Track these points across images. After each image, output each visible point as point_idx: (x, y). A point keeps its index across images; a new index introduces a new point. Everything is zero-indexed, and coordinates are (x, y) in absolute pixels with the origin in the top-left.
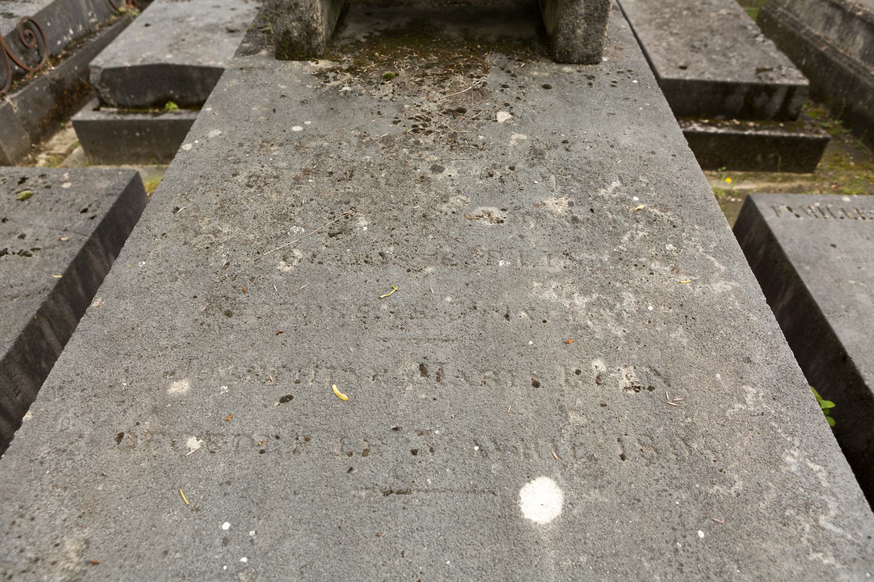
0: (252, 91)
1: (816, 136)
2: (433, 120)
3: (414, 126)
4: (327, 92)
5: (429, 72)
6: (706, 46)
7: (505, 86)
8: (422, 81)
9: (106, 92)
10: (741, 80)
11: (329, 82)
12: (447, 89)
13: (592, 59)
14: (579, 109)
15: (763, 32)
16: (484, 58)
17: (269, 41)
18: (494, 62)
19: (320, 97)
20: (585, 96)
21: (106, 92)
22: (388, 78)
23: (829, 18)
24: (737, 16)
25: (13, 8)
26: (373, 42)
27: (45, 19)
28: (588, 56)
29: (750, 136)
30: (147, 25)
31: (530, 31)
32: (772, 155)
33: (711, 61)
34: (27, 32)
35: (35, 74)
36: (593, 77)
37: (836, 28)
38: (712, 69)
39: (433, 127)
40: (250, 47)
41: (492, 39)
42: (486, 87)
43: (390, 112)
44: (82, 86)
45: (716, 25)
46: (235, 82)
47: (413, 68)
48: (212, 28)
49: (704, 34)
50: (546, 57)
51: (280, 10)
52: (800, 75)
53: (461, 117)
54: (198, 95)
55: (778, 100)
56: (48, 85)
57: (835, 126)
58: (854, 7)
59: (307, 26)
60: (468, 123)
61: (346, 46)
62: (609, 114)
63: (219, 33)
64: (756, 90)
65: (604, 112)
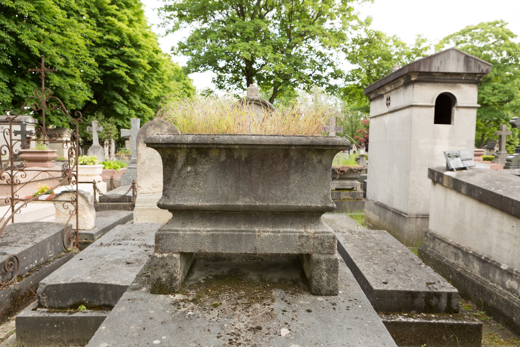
0: (133, 315)
1: (474, 323)
2: (242, 335)
3: (230, 340)
4: (178, 316)
5: (239, 301)
6: (395, 270)
7: (285, 311)
8: (236, 308)
9: (44, 299)
10: (419, 290)
11: (180, 309)
12: (250, 313)
13: (333, 293)
14: (329, 326)
15: (424, 262)
16: (271, 293)
17: (148, 282)
18: (277, 295)
19: (173, 320)
20: (332, 317)
21: (44, 299)
22: (215, 306)
23: (455, 254)
24: (407, 253)
25: (7, 250)
26: (208, 282)
27: (24, 255)
28: (331, 291)
29: (434, 324)
30: (81, 260)
31: (296, 276)
32: (452, 336)
33: (400, 278)
34: (10, 263)
35: (4, 286)
36: (336, 304)
37: (461, 259)
38: (401, 284)
39: (241, 341)
40: (136, 286)
41: (276, 280)
42: (273, 312)
43: (216, 329)
44: (31, 293)
45: (397, 259)
46: (123, 308)
47: (230, 300)
48: (117, 262)
49: (392, 263)
50: (307, 291)
51: (157, 267)
52: (452, 286)
53: (259, 333)
54: (100, 301)
55: (444, 301)
56: (10, 293)
57: (482, 315)
58: (466, 249)
59: (171, 276)
60: (264, 337)
61: (192, 285)
62: (348, 329)
63: (121, 264)
64: (430, 295)
65: (345, 327)
